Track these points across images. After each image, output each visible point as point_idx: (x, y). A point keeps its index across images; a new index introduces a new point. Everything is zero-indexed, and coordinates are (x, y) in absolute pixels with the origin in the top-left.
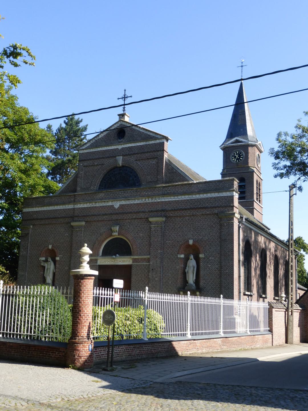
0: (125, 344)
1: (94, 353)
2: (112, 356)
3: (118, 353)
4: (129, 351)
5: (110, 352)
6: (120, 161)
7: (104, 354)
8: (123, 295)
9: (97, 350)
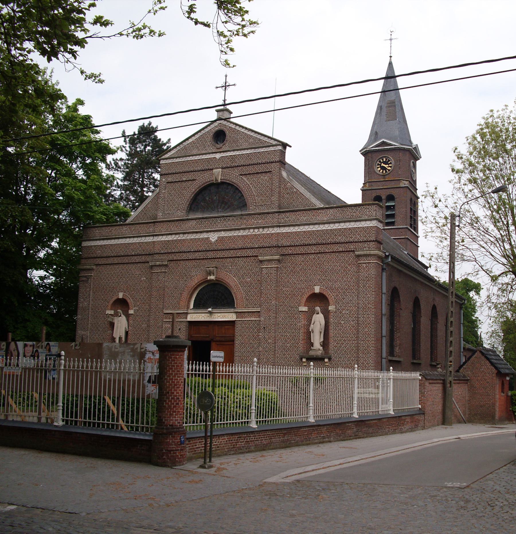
0: (227, 434)
1: (187, 446)
2: (211, 449)
3: (218, 446)
4: (233, 443)
5: (208, 444)
6: (218, 174)
7: (200, 447)
8: (224, 370)
9: (191, 442)
